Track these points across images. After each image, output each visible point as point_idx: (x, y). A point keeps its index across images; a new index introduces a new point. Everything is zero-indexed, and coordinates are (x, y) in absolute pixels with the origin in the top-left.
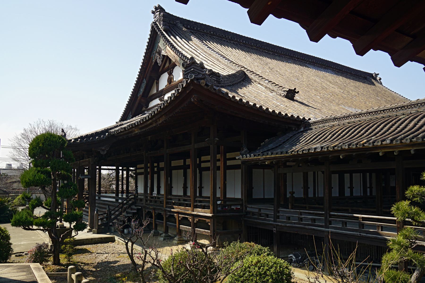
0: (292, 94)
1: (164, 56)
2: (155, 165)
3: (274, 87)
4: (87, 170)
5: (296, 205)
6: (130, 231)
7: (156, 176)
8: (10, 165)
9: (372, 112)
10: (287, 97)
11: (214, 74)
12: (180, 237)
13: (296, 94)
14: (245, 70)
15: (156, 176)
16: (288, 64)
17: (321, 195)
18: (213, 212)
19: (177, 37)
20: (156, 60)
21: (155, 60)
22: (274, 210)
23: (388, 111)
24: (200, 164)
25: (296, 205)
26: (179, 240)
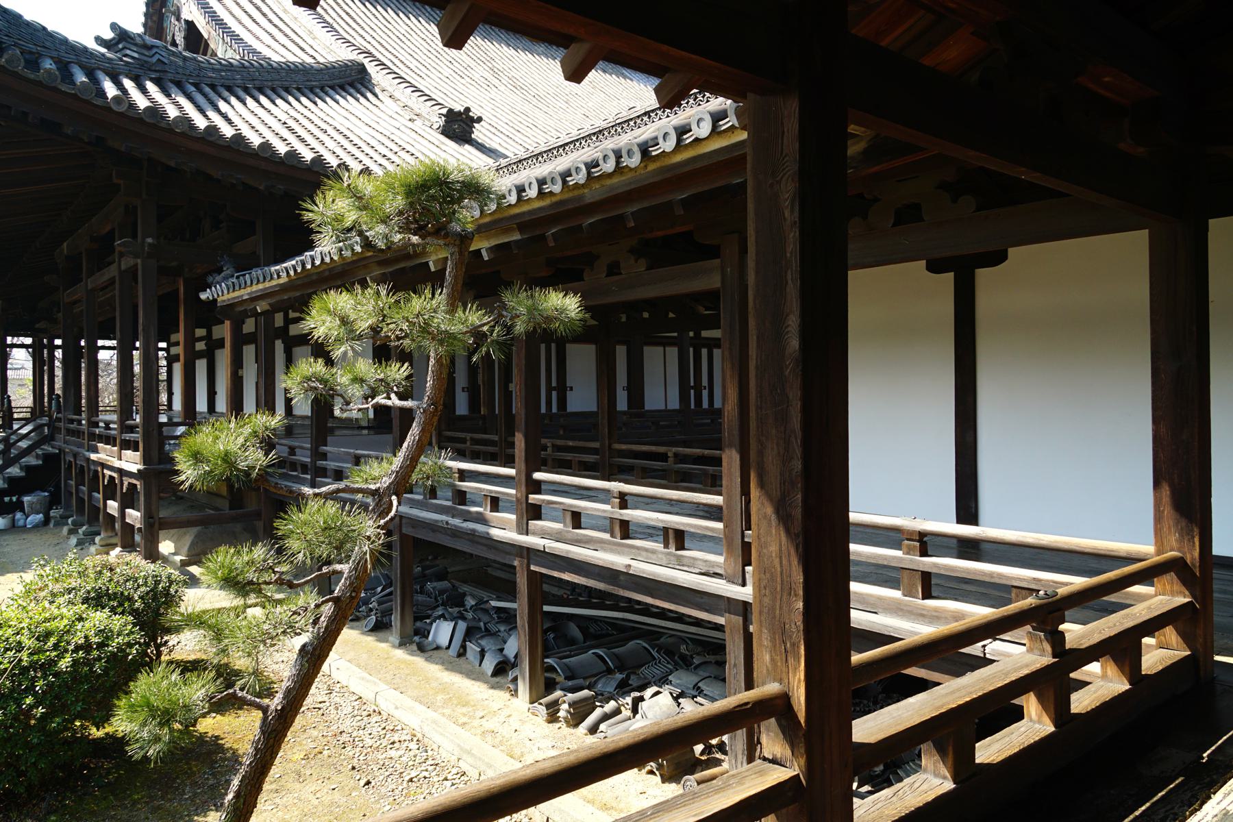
0: (462, 124)
1: (187, 22)
2: (200, 332)
3: (421, 106)
4: (30, 350)
5: (449, 433)
6: (19, 520)
7: (201, 366)
8: (463, 388)
9: (541, 154)
10: (448, 132)
11: (129, 40)
12: (110, 534)
13: (475, 125)
14: (366, 62)
15: (201, 366)
16: (623, 80)
17: (709, 421)
18: (146, 460)
19: (494, 43)
20: (174, 35)
21: (171, 35)
22: (311, 450)
23: (572, 146)
24: (285, 329)
25: (449, 433)
26: (104, 543)
